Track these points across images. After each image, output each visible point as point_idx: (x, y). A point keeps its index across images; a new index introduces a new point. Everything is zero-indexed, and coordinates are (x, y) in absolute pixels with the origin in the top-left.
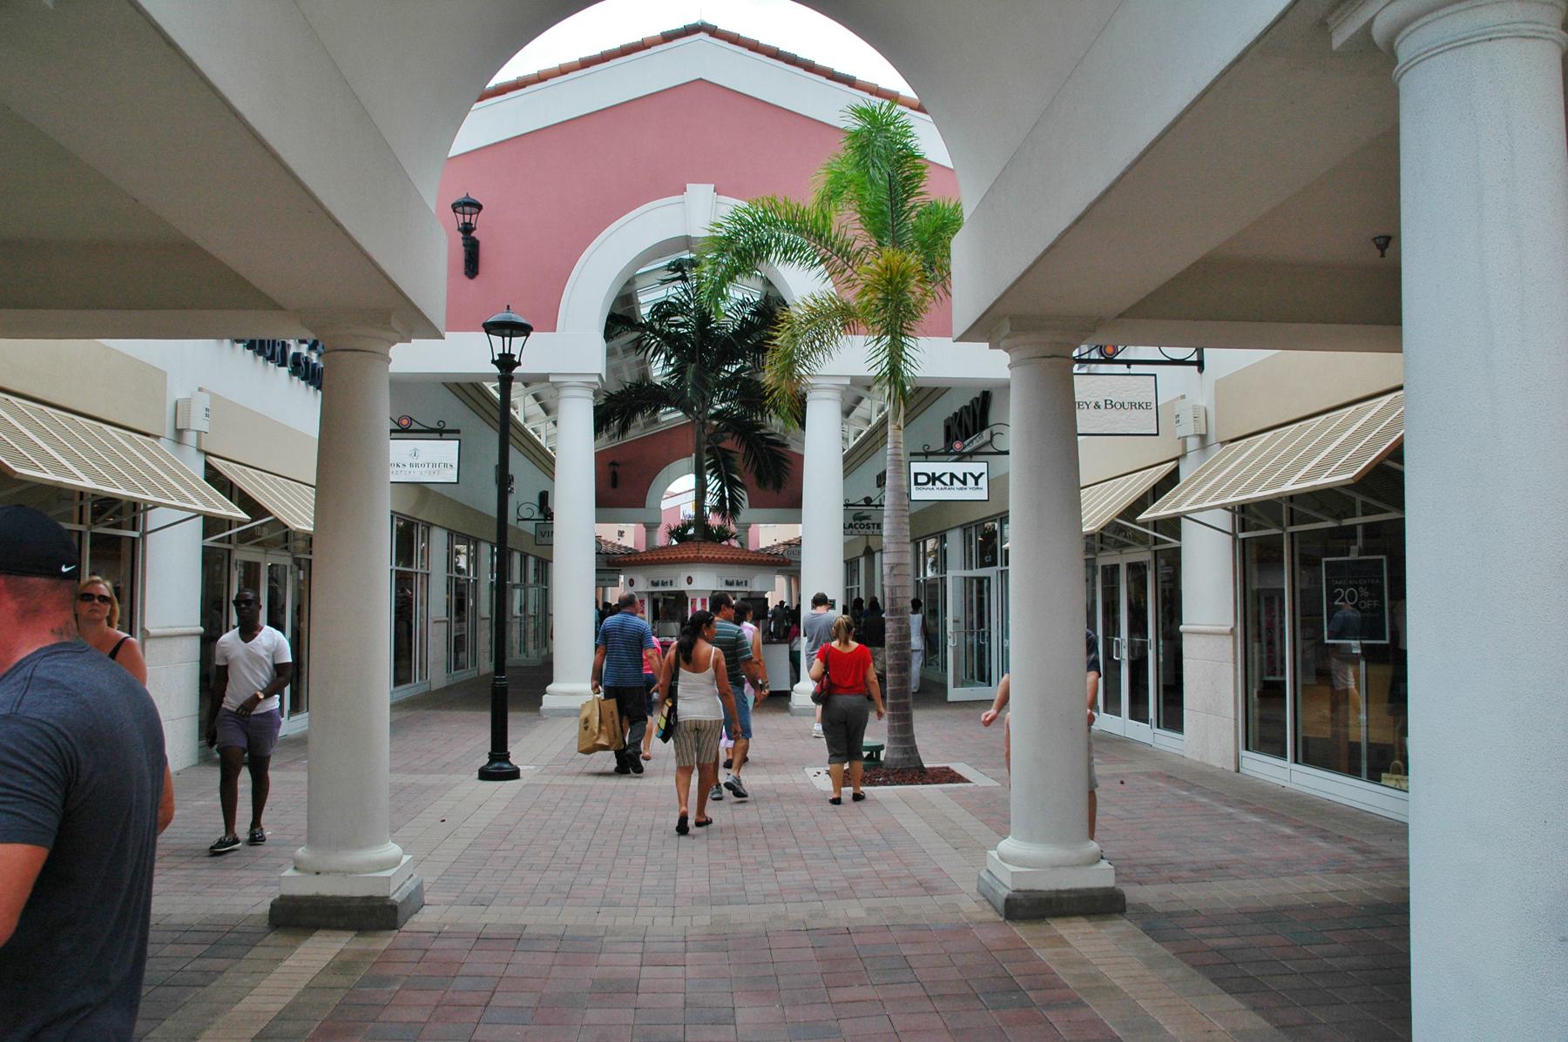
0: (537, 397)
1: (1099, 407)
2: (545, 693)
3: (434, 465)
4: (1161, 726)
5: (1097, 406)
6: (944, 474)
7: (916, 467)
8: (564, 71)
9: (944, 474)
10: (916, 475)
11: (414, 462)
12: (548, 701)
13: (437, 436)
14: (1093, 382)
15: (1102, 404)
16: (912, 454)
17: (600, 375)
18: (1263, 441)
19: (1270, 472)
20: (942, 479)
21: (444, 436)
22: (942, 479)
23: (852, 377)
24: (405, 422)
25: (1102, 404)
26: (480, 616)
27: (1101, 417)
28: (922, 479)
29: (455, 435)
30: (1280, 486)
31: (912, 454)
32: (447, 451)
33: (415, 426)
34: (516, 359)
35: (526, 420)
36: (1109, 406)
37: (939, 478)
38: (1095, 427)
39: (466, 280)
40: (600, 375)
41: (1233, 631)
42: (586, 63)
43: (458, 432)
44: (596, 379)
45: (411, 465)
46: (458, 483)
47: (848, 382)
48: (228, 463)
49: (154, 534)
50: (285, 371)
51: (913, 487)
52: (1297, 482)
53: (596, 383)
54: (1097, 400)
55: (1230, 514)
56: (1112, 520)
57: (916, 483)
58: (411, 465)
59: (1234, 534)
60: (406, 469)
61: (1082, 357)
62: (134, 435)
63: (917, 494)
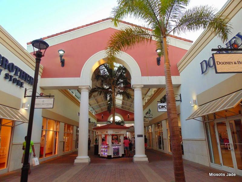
0: (92, 107)
1: (236, 63)
3: (48, 104)
5: (235, 63)
6: (165, 106)
7: (159, 104)
9: (165, 106)
10: (159, 106)
11: (43, 103)
12: (76, 161)
13: (49, 97)
15: (237, 62)
16: (158, 102)
17: (90, 86)
18: (232, 96)
19: (206, 110)
20: (165, 107)
21: (51, 97)
22: (165, 107)
24: (41, 94)
25: (237, 62)
26: (12, 143)
28: (160, 107)
29: (53, 97)
30: (224, 108)
31: (158, 102)
32: (51, 101)
34: (43, 54)
35: (91, 111)
36: (239, 63)
37: (164, 107)
40: (90, 86)
42: (87, 25)
43: (54, 96)
44: (89, 87)
45: (42, 104)
46: (53, 108)
47: (143, 86)
48: (5, 106)
51: (158, 109)
52: (212, 111)
53: (89, 88)
55: (202, 117)
57: (159, 108)
58: (42, 104)
59: (203, 122)
60: (41, 105)
61: (228, 48)
62: (13, 109)
63: (159, 110)
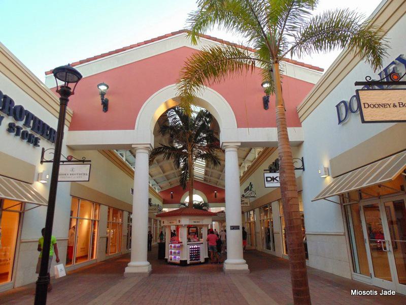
0: (154, 180)
1: (396, 106)
2: (127, 266)
3: (80, 174)
4: (358, 271)
5: (395, 106)
6: (277, 177)
7: (266, 175)
8: (139, 45)
9: (277, 177)
10: (267, 178)
11: (72, 173)
13: (82, 163)
14: (389, 94)
15: (397, 105)
16: (265, 170)
17: (150, 144)
20: (277, 179)
21: (85, 163)
22: (277, 179)
23: (241, 142)
24: (69, 158)
25: (397, 105)
26: (20, 240)
27: (398, 112)
28: (269, 179)
29: (89, 163)
31: (265, 170)
32: (85, 168)
33: (73, 159)
35: (152, 185)
36: (401, 106)
37: (275, 179)
38: (395, 117)
39: (103, 113)
40: (150, 144)
41: (344, 235)
42: (146, 42)
43: (90, 161)
44: (149, 146)
45: (71, 174)
46: (88, 181)
47: (240, 144)
49: (30, 210)
50: (18, 138)
51: (266, 182)
53: (149, 148)
54: (393, 102)
56: (401, 174)
61: (383, 81)
63: (267, 185)
